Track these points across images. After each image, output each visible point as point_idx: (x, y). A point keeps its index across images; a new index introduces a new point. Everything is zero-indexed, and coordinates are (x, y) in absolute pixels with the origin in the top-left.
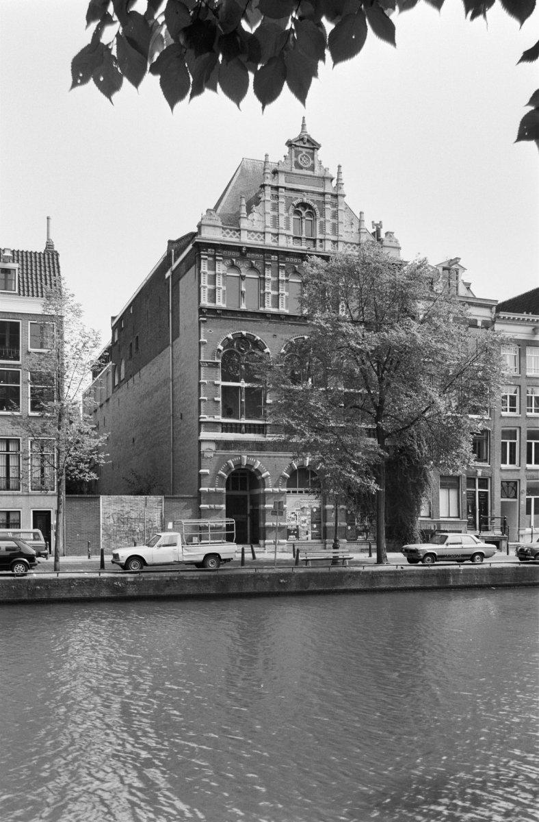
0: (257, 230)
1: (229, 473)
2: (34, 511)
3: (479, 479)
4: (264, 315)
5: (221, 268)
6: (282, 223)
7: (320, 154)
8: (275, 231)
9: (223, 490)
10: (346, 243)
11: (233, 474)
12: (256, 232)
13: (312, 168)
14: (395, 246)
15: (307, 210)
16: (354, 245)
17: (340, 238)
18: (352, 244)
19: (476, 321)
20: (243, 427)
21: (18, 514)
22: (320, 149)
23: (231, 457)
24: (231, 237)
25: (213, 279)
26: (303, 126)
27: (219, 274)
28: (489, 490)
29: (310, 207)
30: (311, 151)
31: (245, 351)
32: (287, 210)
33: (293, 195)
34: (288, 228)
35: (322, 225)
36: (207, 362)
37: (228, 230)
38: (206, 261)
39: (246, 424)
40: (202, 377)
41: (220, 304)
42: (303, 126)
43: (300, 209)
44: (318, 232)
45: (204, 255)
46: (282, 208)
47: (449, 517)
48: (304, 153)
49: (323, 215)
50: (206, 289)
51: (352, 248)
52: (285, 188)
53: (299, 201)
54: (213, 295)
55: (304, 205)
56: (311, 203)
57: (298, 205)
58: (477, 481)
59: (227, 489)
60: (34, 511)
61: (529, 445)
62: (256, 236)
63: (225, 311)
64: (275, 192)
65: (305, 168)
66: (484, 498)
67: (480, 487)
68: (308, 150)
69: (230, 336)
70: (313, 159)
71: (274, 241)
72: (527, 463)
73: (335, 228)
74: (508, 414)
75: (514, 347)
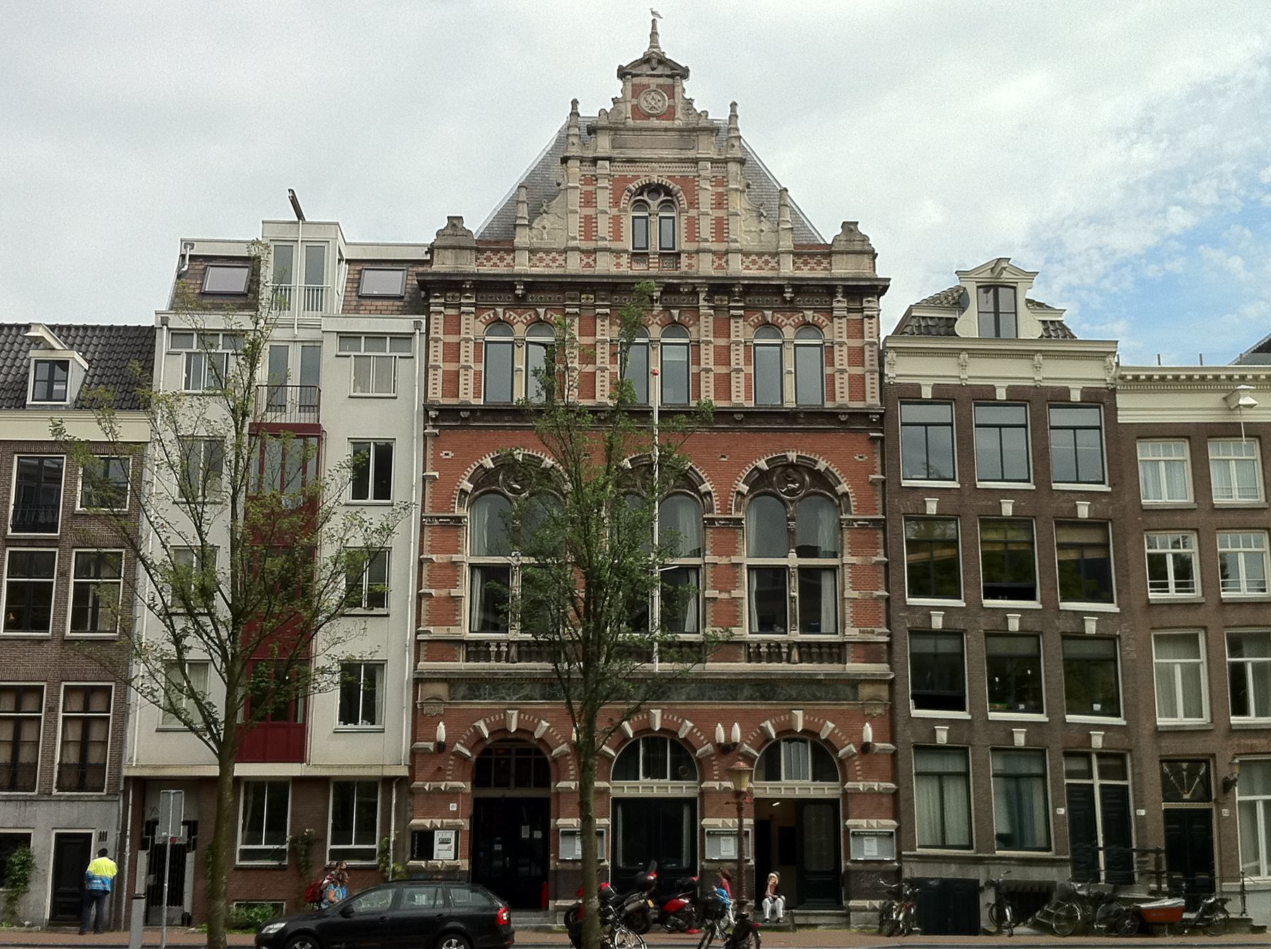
0: (749, 248)
1: (480, 748)
2: (58, 835)
3: (1101, 755)
4: (832, 416)
5: (741, 331)
6: (603, 227)
7: (690, 88)
8: (722, 247)
9: (466, 786)
10: (746, 254)
11: (487, 751)
12: (548, 252)
13: (670, 114)
14: (858, 248)
15: (663, 198)
16: (766, 257)
17: (734, 246)
18: (760, 255)
19: (1067, 390)
20: (514, 649)
21: (1044, 845)
22: (691, 74)
23: (482, 715)
24: (495, 265)
25: (723, 356)
26: (654, 34)
27: (738, 343)
28: (1129, 783)
29: (668, 192)
30: (670, 81)
31: (523, 490)
32: (616, 203)
33: (629, 171)
34: (617, 236)
35: (693, 224)
36: (438, 518)
37: (488, 253)
38: (442, 316)
39: (800, 645)
40: (426, 548)
41: (740, 398)
42: (654, 34)
43: (645, 197)
44: (684, 239)
45: (436, 304)
46: (603, 199)
47: (944, 846)
48: (653, 87)
49: (693, 204)
50: (440, 372)
51: (760, 262)
52: (610, 159)
53: (643, 181)
54: (724, 385)
55: (654, 189)
56: (665, 181)
57: (641, 190)
58: (1094, 758)
59: (477, 783)
60: (58, 835)
61: (1238, 673)
62: (548, 259)
63: (749, 415)
64: (589, 170)
65: (653, 115)
66: (1117, 800)
67: (1102, 776)
68: (661, 81)
69: (762, 464)
70: (672, 96)
71: (720, 267)
72: (1234, 714)
73: (720, 228)
74: (1172, 594)
75: (1181, 452)
